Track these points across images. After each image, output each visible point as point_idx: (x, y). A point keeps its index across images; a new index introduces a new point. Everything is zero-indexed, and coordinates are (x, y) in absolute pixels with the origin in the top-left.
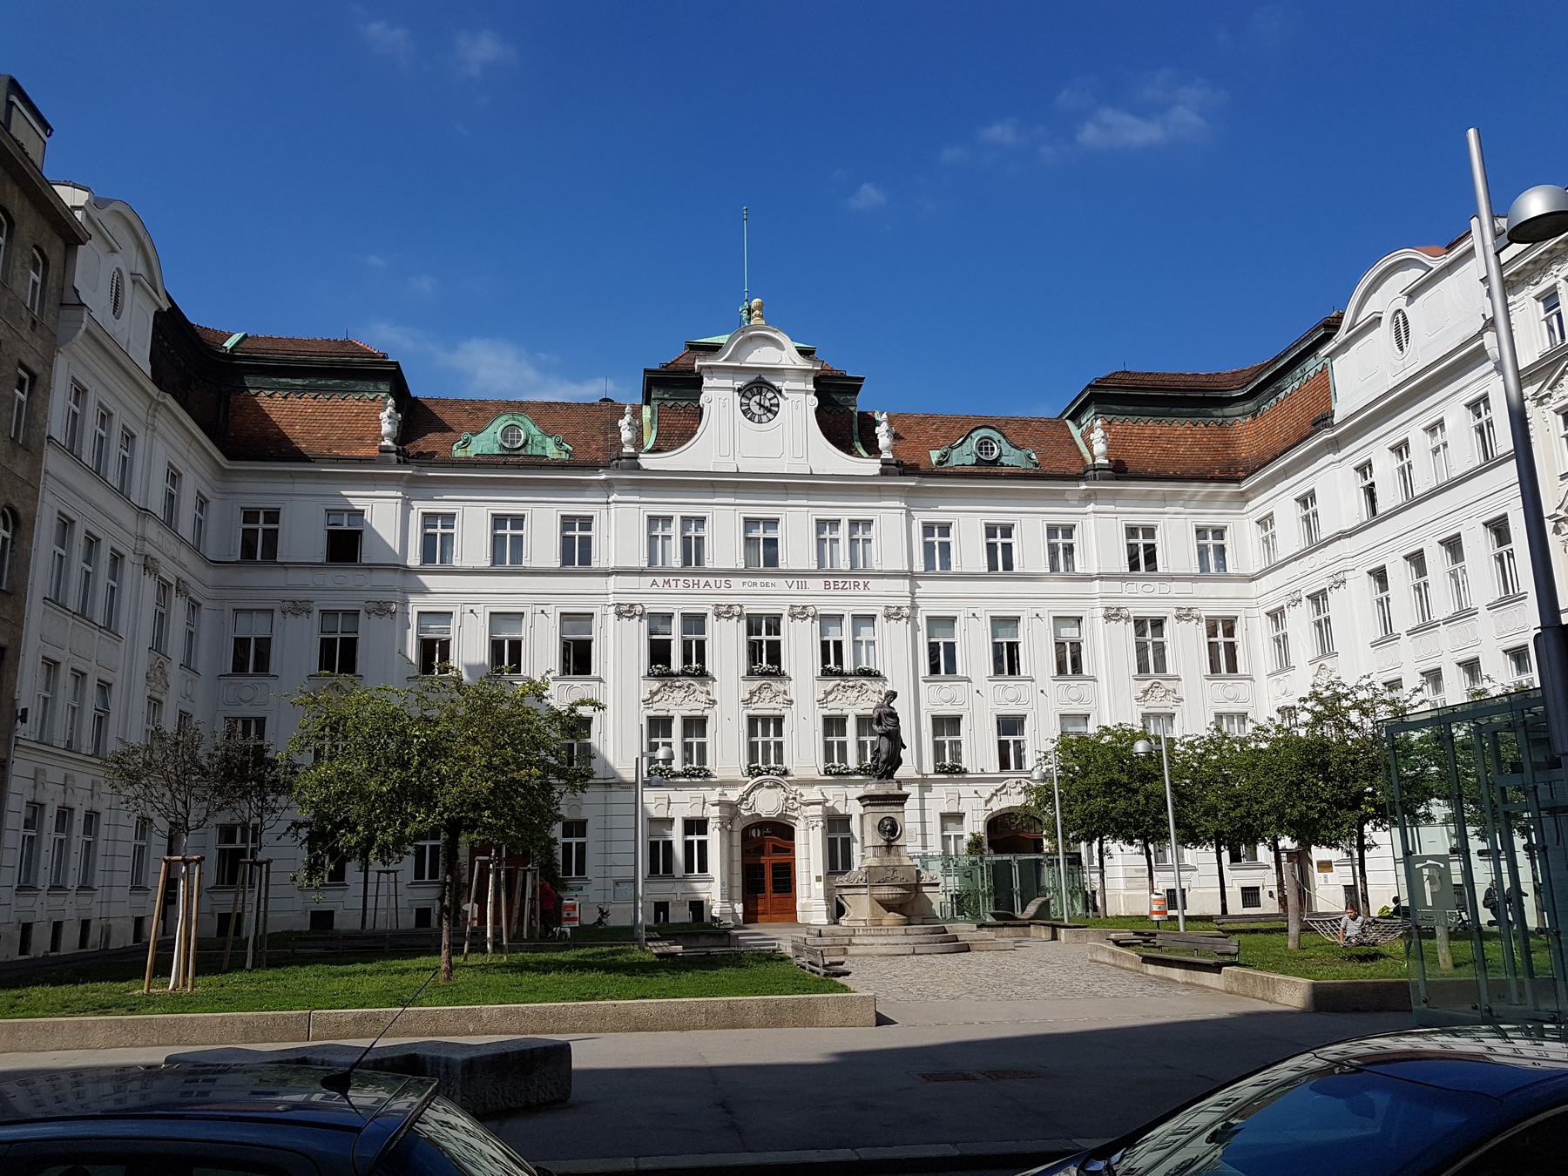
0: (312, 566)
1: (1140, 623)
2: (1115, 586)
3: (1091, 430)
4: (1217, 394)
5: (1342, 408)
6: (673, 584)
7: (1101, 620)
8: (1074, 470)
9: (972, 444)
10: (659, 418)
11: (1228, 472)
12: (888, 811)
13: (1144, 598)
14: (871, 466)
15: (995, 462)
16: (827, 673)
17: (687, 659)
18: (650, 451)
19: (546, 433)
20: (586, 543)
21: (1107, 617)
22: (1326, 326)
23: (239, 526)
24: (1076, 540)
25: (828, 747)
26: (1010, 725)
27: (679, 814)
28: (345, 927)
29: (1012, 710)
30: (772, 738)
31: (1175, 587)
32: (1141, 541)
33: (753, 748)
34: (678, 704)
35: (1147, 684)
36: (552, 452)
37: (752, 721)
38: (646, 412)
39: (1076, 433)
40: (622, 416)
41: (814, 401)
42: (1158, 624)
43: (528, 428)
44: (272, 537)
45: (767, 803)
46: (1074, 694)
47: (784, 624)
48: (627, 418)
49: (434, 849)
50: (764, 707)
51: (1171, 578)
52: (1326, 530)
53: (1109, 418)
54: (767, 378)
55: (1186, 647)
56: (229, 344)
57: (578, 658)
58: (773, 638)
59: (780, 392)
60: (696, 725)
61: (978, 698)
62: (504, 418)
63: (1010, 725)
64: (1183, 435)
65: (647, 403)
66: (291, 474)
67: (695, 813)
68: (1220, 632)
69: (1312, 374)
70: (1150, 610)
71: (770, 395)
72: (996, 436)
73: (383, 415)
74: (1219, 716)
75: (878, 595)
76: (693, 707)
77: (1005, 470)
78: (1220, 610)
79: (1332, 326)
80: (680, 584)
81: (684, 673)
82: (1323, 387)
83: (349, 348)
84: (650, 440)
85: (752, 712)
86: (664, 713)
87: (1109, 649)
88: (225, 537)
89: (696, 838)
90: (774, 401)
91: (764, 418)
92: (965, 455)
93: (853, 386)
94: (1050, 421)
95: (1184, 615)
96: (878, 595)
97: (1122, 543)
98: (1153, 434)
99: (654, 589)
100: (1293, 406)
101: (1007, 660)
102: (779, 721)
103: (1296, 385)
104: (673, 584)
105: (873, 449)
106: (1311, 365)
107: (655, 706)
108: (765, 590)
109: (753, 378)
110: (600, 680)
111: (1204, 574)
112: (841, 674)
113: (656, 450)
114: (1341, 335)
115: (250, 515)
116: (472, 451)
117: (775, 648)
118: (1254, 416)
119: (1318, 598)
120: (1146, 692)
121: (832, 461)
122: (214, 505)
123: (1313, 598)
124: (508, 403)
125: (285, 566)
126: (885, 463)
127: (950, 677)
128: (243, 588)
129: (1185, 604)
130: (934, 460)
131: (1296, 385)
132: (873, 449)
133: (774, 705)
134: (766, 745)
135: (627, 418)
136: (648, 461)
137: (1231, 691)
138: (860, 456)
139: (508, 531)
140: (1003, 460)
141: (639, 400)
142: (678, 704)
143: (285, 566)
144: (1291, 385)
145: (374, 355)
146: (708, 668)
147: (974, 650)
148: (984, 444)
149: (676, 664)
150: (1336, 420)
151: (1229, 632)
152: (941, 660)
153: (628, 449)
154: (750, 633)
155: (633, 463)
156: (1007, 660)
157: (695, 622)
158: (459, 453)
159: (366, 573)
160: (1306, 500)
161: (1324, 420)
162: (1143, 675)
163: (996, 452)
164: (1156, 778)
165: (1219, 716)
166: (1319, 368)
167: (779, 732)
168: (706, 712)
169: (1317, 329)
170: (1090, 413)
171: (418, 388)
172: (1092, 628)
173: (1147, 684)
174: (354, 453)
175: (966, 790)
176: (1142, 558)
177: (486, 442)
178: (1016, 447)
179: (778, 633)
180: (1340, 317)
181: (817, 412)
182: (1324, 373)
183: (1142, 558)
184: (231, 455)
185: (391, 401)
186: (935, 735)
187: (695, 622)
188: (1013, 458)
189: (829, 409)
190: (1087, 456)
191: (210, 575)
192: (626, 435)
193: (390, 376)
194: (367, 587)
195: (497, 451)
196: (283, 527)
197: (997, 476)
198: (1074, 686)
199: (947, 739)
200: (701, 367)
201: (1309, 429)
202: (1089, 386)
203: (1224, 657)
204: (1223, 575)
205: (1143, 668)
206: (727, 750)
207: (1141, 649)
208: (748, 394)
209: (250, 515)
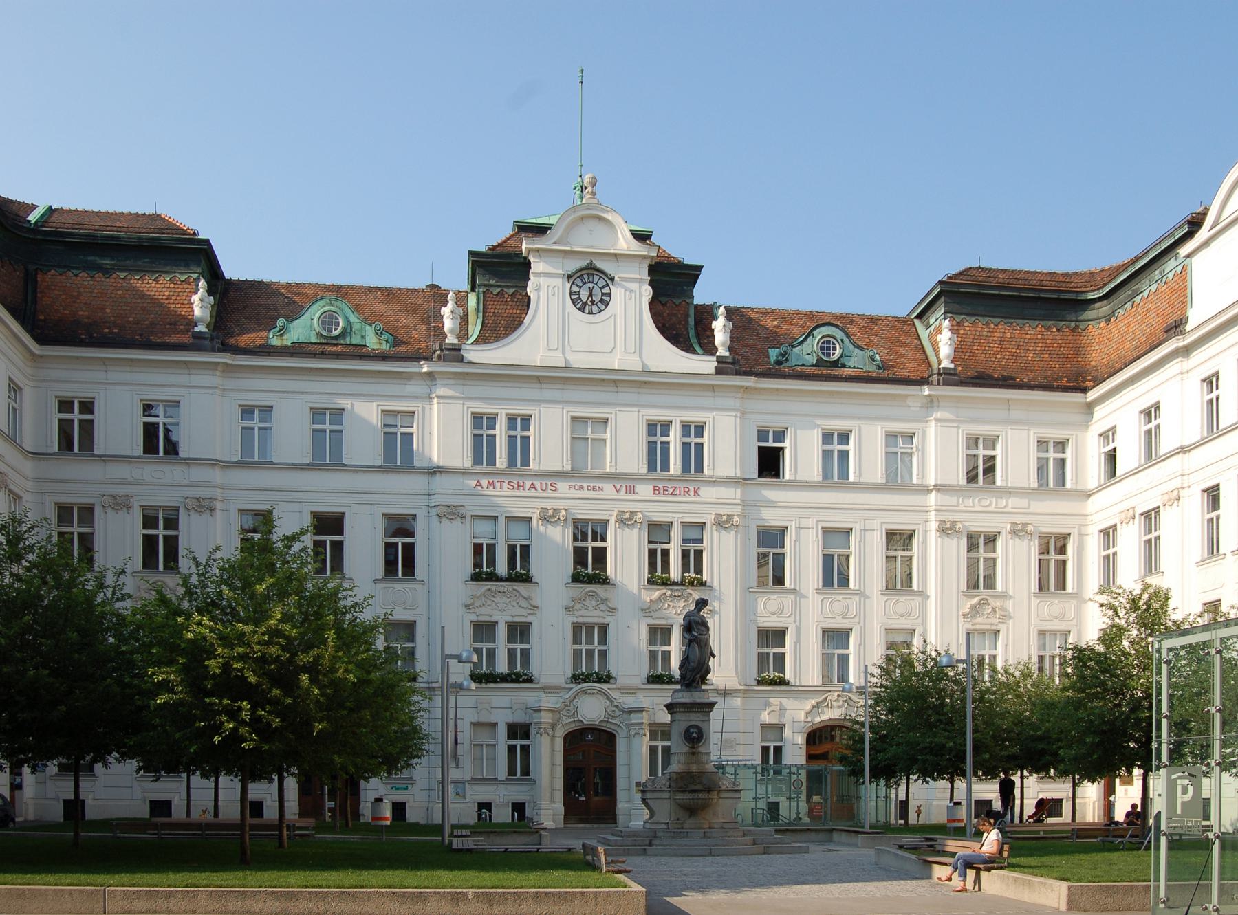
0: (130, 459)
3: (939, 331)
4: (1073, 296)
5: (1198, 315)
6: (498, 485)
8: (916, 374)
9: (813, 344)
10: (484, 308)
11: (1076, 379)
12: (694, 718)
13: (980, 512)
14: (706, 365)
15: (835, 364)
16: (476, 577)
17: (685, 567)
18: (476, 342)
19: (366, 321)
22: (1189, 223)
23: (55, 417)
25: (763, 658)
26: (835, 637)
28: (93, 818)
29: (839, 623)
30: (596, 647)
31: (1013, 502)
33: (577, 654)
34: (502, 609)
35: (975, 601)
36: (372, 341)
37: (577, 628)
38: (472, 300)
39: (924, 334)
40: (445, 303)
41: (647, 292)
42: (991, 540)
43: (346, 315)
44: (88, 428)
45: (591, 710)
46: (901, 608)
48: (450, 305)
49: (666, 750)
51: (1009, 491)
52: (1167, 443)
53: (959, 318)
54: (599, 264)
55: (1016, 564)
56: (33, 217)
57: (400, 560)
58: (599, 544)
59: (612, 279)
60: (519, 631)
61: (805, 611)
62: (321, 303)
63: (835, 637)
64: (1032, 339)
65: (473, 290)
66: (103, 361)
68: (590, 539)
69: (1170, 276)
70: (982, 525)
72: (839, 334)
73: (195, 299)
74: (1042, 634)
75: (709, 502)
77: (846, 371)
78: (1053, 527)
79: (1195, 224)
80: (505, 485)
81: (682, 583)
82: (1181, 292)
83: (158, 223)
84: (475, 330)
85: (575, 620)
87: (938, 561)
88: (40, 427)
90: (606, 290)
92: (808, 352)
93: (692, 273)
94: (897, 320)
95: (1018, 531)
96: (709, 502)
98: (1004, 337)
99: (533, 493)
100: (1148, 312)
101: (834, 574)
102: (604, 629)
103: (1153, 288)
104: (498, 485)
105: (710, 349)
106: (1171, 265)
107: (478, 611)
108: (592, 494)
109: (583, 263)
110: (858, 593)
111: (316, 465)
112: (665, 583)
113: (482, 340)
114: (1203, 234)
115: (65, 405)
116: (287, 340)
117: (600, 555)
118: (1108, 321)
119: (1150, 517)
120: (973, 608)
121: (666, 357)
122: (28, 395)
123: (1147, 515)
124: (326, 288)
125: (104, 459)
126: (720, 360)
127: (843, 590)
128: (61, 481)
129: (1019, 519)
130: (773, 359)
131: (1153, 288)
132: (710, 349)
133: (989, 621)
134: (590, 653)
135: (450, 305)
136: (476, 354)
138: (694, 352)
139: (257, 424)
141: (464, 286)
142: (502, 609)
143: (104, 459)
144: (1149, 288)
145: (184, 232)
146: (534, 571)
147: (803, 558)
148: (827, 346)
149: (675, 573)
150: (1188, 328)
151: (1062, 550)
152: (771, 567)
153: (451, 339)
154: (575, 539)
155: (454, 354)
156: (834, 574)
157: (694, 530)
158: (276, 341)
159: (184, 468)
160: (1150, 413)
161: (1176, 327)
162: (974, 592)
163: (838, 352)
165: (1042, 634)
166: (1179, 269)
167: (603, 639)
168: (529, 619)
169: (1180, 227)
170: (940, 311)
171: (232, 269)
172: (925, 542)
173: (975, 601)
174: (167, 339)
176: (981, 471)
177: (303, 329)
178: (859, 347)
179: (604, 539)
180: (1204, 215)
181: (651, 304)
182: (1184, 275)
183: (981, 471)
184: (41, 340)
185: (202, 283)
187: (694, 530)
188: (857, 360)
189: (664, 300)
190: (933, 359)
191: (28, 467)
192: (448, 324)
193: (193, 253)
194: (186, 482)
195: (314, 340)
196: (99, 417)
197: (837, 379)
198: (903, 603)
200: (529, 251)
201: (1161, 336)
202: (941, 282)
203: (1053, 573)
204: (339, 466)
206: (552, 657)
208: (579, 282)
209: (65, 405)
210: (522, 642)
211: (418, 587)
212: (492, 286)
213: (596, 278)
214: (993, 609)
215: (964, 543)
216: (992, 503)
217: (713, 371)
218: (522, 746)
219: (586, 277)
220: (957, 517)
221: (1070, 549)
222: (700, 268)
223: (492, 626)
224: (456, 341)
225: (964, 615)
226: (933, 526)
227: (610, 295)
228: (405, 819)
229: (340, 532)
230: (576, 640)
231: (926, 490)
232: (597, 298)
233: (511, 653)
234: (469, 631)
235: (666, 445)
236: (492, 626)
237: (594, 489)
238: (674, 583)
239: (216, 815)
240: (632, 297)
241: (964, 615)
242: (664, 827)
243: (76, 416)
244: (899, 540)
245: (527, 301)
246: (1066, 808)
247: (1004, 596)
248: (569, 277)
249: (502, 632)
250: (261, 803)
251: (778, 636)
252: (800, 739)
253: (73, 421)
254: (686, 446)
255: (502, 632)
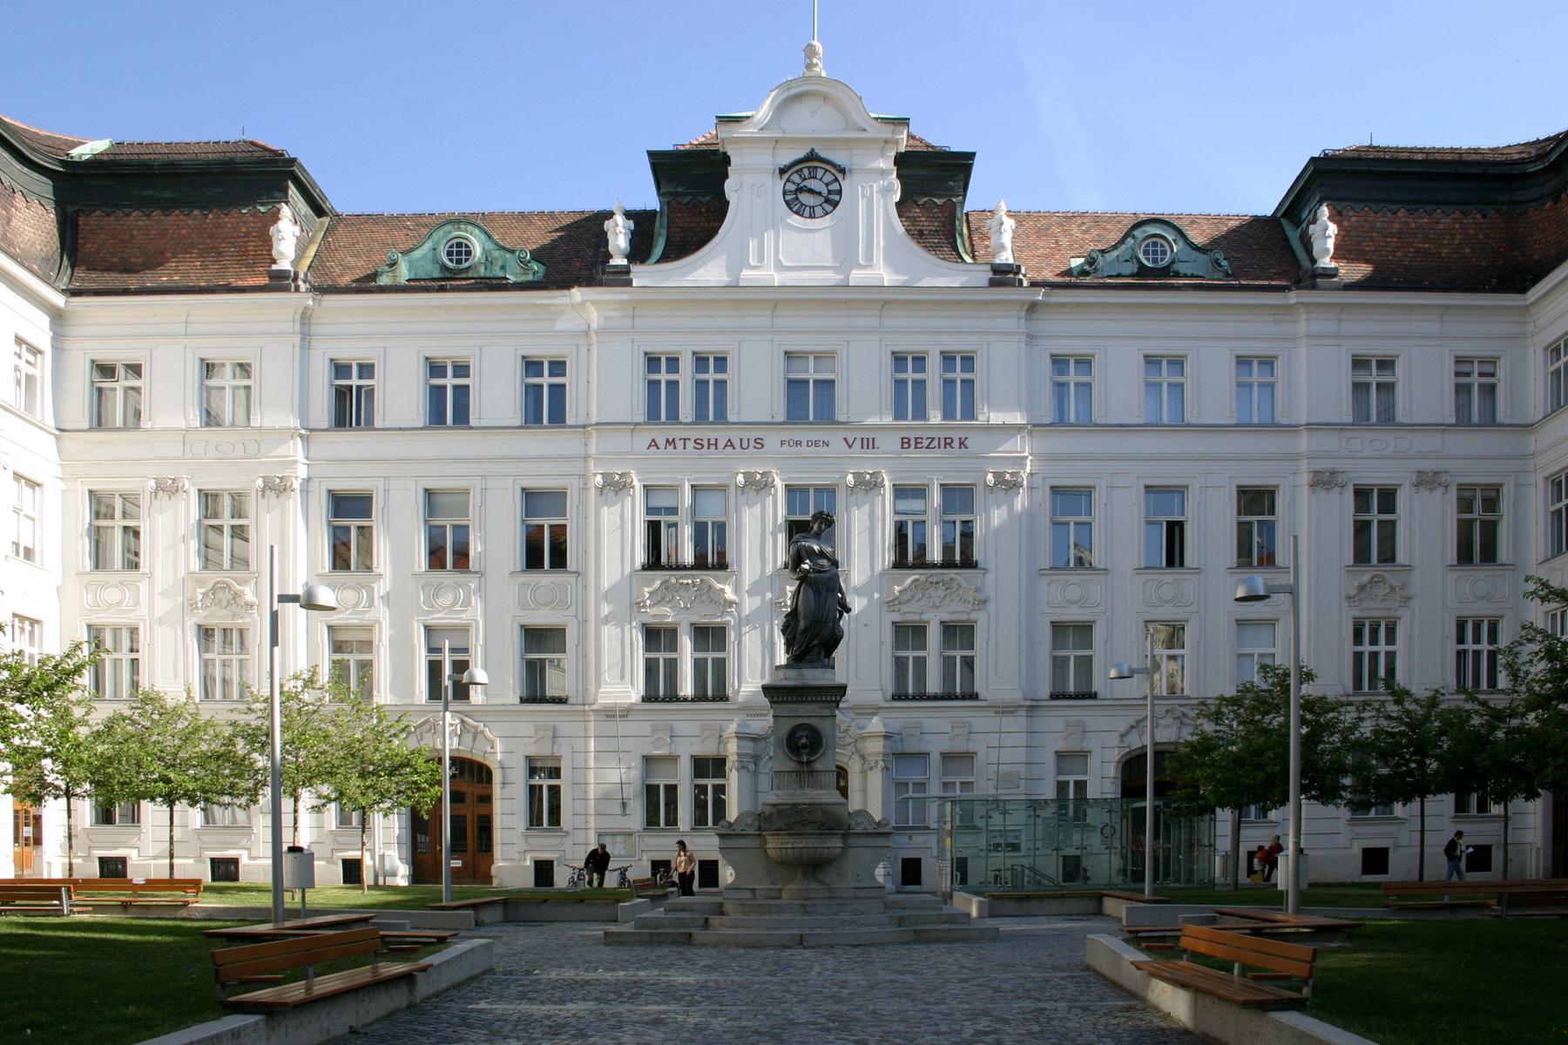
1: (1362, 495)
2: (1329, 442)
6: (680, 444)
7: (1305, 490)
20: (558, 392)
21: (1314, 485)
24: (978, 377)
25: (900, 664)
27: (687, 750)
30: (1382, 648)
32: (449, 381)
35: (1365, 578)
46: (1074, 593)
47: (251, 505)
50: (1374, 609)
60: (958, 633)
67: (708, 749)
70: (1375, 475)
71: (828, 178)
76: (954, 612)
86: (915, 618)
89: (710, 782)
90: (835, 187)
91: (818, 211)
95: (1427, 481)
97: (1345, 377)
107: (904, 608)
110: (480, 574)
120: (1362, 588)
129: (1428, 465)
137: (113, 595)
140: (1179, 267)
164: (1277, 708)
167: (1391, 639)
168: (973, 616)
175: (982, 722)
186: (1055, 646)
195: (436, 274)
199: (1072, 654)
205: (1361, 555)
207: (1361, 529)
210: (914, 648)
211: (572, 579)
212: (679, 194)
213: (820, 173)
214: (1392, 588)
215: (1349, 495)
216: (1387, 441)
217: (985, 283)
218: (1076, 782)
219: (806, 172)
220: (1338, 465)
221: (1505, 506)
222: (971, 156)
223: (919, 631)
224: (625, 262)
225: (1348, 598)
226: (1304, 479)
227: (840, 192)
228: (488, 878)
229: (367, 514)
230: (1461, 639)
231: (1292, 428)
232: (804, 198)
233: (948, 663)
234: (888, 634)
235: (673, 386)
236: (919, 631)
237: (816, 443)
238: (934, 566)
239: (1505, 876)
240: (875, 194)
241: (1348, 598)
242: (748, 894)
243: (546, 380)
244: (1256, 500)
245: (725, 204)
246: (1497, 857)
247: (1408, 568)
248: (782, 171)
249: (934, 635)
250: (919, 860)
251: (1083, 631)
252: (1112, 770)
253: (445, 387)
254: (701, 385)
255: (934, 635)
